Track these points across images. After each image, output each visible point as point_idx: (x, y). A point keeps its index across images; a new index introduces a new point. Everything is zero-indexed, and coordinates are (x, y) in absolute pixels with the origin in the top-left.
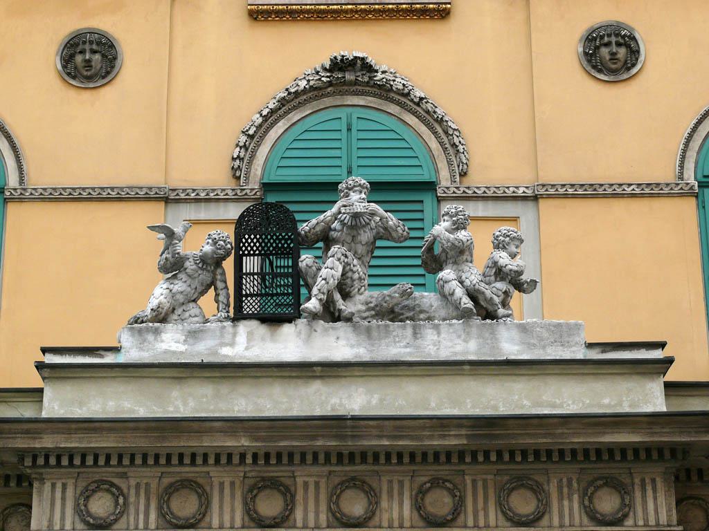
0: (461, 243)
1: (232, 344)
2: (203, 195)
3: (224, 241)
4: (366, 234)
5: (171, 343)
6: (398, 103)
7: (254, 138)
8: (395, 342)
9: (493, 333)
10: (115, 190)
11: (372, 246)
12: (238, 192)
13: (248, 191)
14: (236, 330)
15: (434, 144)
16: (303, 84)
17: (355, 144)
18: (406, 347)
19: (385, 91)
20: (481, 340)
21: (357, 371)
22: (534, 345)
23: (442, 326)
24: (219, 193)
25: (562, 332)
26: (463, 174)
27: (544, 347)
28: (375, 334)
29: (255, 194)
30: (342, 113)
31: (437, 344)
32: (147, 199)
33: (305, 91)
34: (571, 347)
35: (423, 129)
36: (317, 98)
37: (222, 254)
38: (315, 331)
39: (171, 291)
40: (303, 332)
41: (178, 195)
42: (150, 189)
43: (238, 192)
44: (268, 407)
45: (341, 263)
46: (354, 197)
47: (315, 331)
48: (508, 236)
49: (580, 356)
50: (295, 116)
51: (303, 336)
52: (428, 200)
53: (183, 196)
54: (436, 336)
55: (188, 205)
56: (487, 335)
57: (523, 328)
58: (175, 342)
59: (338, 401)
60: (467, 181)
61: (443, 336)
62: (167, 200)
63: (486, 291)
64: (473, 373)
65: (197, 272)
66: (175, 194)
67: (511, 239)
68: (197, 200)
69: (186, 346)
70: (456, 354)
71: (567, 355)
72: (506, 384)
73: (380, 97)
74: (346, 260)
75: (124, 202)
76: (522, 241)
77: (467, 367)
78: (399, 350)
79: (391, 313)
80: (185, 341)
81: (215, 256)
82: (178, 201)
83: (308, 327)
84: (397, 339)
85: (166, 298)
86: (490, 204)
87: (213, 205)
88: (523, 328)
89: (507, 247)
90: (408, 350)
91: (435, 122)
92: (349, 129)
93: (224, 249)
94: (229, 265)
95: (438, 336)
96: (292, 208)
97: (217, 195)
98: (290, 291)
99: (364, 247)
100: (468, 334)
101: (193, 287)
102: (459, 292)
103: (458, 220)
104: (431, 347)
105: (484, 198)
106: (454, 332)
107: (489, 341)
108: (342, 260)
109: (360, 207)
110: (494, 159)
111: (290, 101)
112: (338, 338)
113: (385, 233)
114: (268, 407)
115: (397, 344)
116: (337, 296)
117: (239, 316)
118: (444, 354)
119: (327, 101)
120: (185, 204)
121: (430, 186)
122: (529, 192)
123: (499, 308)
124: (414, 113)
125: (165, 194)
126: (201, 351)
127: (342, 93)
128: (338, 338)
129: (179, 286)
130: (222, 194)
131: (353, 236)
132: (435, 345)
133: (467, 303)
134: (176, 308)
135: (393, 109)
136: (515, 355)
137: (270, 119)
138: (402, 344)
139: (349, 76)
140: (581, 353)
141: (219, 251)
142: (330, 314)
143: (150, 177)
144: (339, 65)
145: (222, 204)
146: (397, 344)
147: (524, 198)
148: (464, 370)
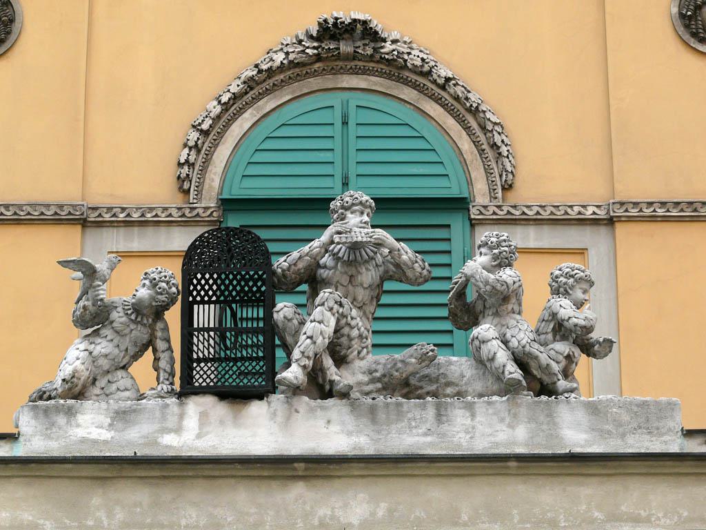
0: (505, 287)
1: (178, 430)
2: (136, 216)
3: (168, 283)
4: (370, 273)
5: (91, 428)
6: (415, 86)
7: (208, 135)
8: (410, 428)
9: (550, 415)
10: (10, 208)
11: (378, 291)
12: (187, 211)
13: (201, 211)
14: (183, 410)
15: (466, 144)
16: (279, 58)
17: (337, 157)
18: (425, 435)
19: (395, 68)
20: (533, 425)
21: (356, 470)
22: (609, 433)
23: (477, 405)
24: (159, 214)
25: (649, 414)
26: (507, 188)
27: (623, 436)
28: (382, 416)
29: (211, 215)
30: (335, 99)
31: (470, 431)
32: (57, 221)
33: (282, 68)
34: (662, 435)
35: (450, 123)
36: (298, 78)
37: (163, 301)
38: (297, 411)
39: (91, 353)
40: (279, 413)
41: (100, 215)
42: (61, 207)
43: (187, 211)
44: (229, 520)
45: (334, 315)
46: (353, 219)
47: (297, 411)
48: (572, 276)
49: (674, 449)
50: (268, 104)
51: (279, 419)
52: (458, 224)
53: (107, 217)
54: (470, 419)
55: (115, 229)
56: (542, 418)
57: (594, 409)
58: (96, 427)
59: (329, 513)
60: (513, 198)
61: (478, 419)
62: (84, 223)
63: (540, 354)
64: (522, 472)
65: (128, 326)
66: (97, 214)
67: (576, 281)
68: (128, 224)
69: (113, 432)
70: (497, 444)
71: (656, 447)
72: (569, 488)
73: (389, 76)
74: (341, 310)
75: (23, 226)
76: (592, 284)
77: (513, 464)
78: (417, 438)
79: (405, 387)
80: (110, 425)
81: (154, 304)
82: (100, 224)
83: (286, 405)
84: (414, 424)
85: (83, 364)
86: (546, 229)
87: (150, 230)
88: (594, 409)
89: (571, 292)
90: (429, 439)
91: (467, 112)
92: (345, 123)
93: (167, 293)
94: (173, 316)
95: (472, 420)
96: (264, 234)
97: (156, 216)
98: (261, 354)
99: (367, 292)
100: (515, 416)
101: (123, 347)
102: (502, 357)
103: (500, 253)
104: (462, 435)
105: (538, 221)
106: (495, 414)
107: (545, 427)
108: (335, 310)
109: (360, 235)
110: (552, 166)
111: (261, 83)
112: (329, 422)
113: (397, 271)
114: (229, 520)
115: (413, 432)
116: (328, 362)
117: (188, 390)
118: (481, 446)
119: (314, 83)
120: (111, 229)
121: (459, 204)
122: (602, 214)
123: (559, 380)
124: (438, 100)
125: (82, 214)
126: (133, 439)
127: (335, 72)
128: (329, 422)
129: (102, 347)
130: (163, 215)
131: (351, 276)
132: (467, 432)
133: (512, 371)
134: (98, 377)
135: (408, 93)
136: (582, 447)
137: (232, 107)
138: (420, 431)
139: (346, 47)
140: (675, 445)
141: (159, 297)
142: (319, 387)
143: (59, 189)
144: (331, 31)
145: (163, 229)
146: (413, 432)
147: (595, 222)
148: (508, 468)
